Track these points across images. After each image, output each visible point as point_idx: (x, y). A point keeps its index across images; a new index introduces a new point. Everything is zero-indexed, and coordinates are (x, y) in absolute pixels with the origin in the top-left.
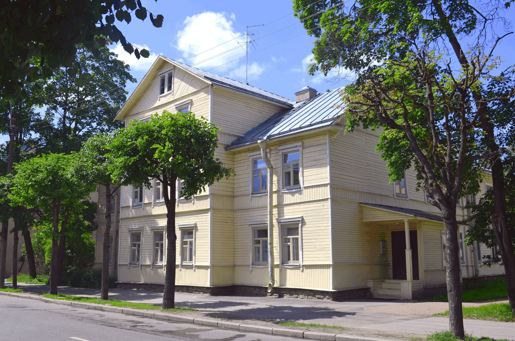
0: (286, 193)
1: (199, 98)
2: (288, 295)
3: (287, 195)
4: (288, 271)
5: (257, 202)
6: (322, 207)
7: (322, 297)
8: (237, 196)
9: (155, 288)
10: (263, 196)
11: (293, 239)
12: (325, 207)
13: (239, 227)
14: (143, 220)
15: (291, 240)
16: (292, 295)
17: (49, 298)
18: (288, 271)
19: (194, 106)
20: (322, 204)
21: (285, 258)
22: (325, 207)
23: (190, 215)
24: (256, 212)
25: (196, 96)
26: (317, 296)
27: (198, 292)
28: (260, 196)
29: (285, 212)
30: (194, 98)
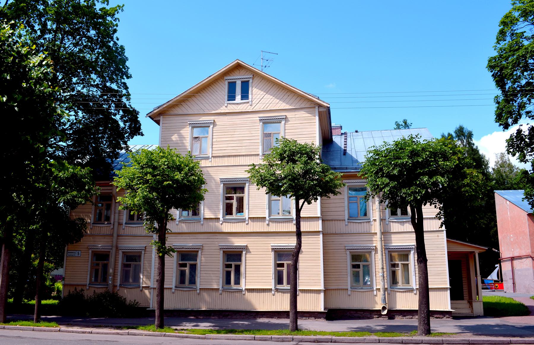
0: (393, 222)
1: (297, 116)
2: (401, 317)
3: (394, 224)
4: (398, 294)
5: (355, 227)
6: (437, 238)
7: (441, 316)
8: (327, 220)
9: (228, 315)
10: (364, 222)
11: (404, 264)
12: (440, 237)
13: (333, 251)
14: (202, 237)
15: (400, 265)
16: (405, 316)
17: (451, 337)
18: (398, 294)
19: (289, 123)
20: (437, 235)
21: (125, 276)
22: (440, 237)
23: (258, 236)
24: (353, 237)
25: (293, 113)
26: (435, 316)
27: (306, 317)
28: (361, 223)
29: (392, 239)
30: (289, 115)
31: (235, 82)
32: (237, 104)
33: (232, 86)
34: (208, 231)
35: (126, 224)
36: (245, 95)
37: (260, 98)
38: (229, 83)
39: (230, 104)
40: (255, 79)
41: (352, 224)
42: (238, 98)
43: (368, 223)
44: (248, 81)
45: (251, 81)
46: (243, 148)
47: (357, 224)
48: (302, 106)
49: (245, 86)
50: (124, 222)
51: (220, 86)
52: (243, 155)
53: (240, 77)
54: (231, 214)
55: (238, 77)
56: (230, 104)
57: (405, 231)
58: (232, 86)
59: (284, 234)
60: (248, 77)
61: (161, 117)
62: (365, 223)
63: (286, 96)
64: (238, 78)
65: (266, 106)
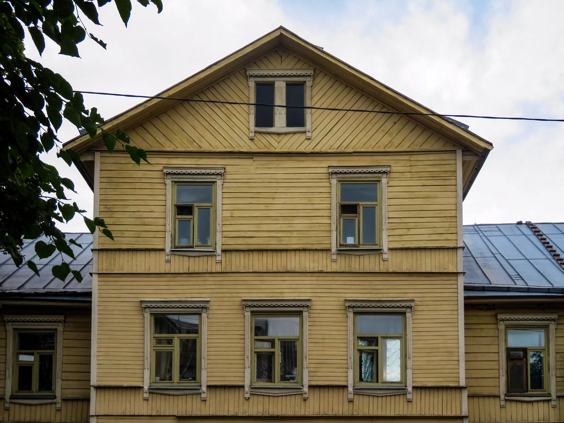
28: (532, 402)
31: (272, 84)
32: (279, 134)
33: (265, 92)
34: (218, 414)
35: (12, 397)
36: (296, 118)
37: (332, 126)
38: (258, 84)
39: (260, 133)
40: (318, 79)
41: (514, 404)
42: (280, 117)
43: (546, 405)
44: (303, 84)
45: (309, 84)
46: (295, 234)
47: (525, 405)
48: (426, 147)
49: (296, 91)
50: (8, 393)
51: (232, 86)
52: (295, 250)
53: (285, 72)
54: (270, 378)
55: (280, 73)
56: (260, 133)
57: (427, 414)
58: (265, 92)
59: (419, 275)
60: (303, 73)
61: (98, 155)
62: (541, 404)
63: (389, 124)
64: (280, 72)
65: (345, 144)
